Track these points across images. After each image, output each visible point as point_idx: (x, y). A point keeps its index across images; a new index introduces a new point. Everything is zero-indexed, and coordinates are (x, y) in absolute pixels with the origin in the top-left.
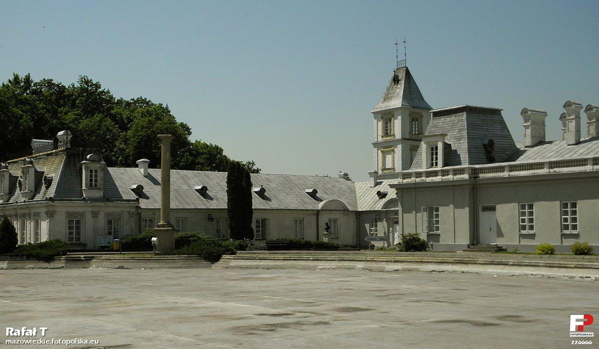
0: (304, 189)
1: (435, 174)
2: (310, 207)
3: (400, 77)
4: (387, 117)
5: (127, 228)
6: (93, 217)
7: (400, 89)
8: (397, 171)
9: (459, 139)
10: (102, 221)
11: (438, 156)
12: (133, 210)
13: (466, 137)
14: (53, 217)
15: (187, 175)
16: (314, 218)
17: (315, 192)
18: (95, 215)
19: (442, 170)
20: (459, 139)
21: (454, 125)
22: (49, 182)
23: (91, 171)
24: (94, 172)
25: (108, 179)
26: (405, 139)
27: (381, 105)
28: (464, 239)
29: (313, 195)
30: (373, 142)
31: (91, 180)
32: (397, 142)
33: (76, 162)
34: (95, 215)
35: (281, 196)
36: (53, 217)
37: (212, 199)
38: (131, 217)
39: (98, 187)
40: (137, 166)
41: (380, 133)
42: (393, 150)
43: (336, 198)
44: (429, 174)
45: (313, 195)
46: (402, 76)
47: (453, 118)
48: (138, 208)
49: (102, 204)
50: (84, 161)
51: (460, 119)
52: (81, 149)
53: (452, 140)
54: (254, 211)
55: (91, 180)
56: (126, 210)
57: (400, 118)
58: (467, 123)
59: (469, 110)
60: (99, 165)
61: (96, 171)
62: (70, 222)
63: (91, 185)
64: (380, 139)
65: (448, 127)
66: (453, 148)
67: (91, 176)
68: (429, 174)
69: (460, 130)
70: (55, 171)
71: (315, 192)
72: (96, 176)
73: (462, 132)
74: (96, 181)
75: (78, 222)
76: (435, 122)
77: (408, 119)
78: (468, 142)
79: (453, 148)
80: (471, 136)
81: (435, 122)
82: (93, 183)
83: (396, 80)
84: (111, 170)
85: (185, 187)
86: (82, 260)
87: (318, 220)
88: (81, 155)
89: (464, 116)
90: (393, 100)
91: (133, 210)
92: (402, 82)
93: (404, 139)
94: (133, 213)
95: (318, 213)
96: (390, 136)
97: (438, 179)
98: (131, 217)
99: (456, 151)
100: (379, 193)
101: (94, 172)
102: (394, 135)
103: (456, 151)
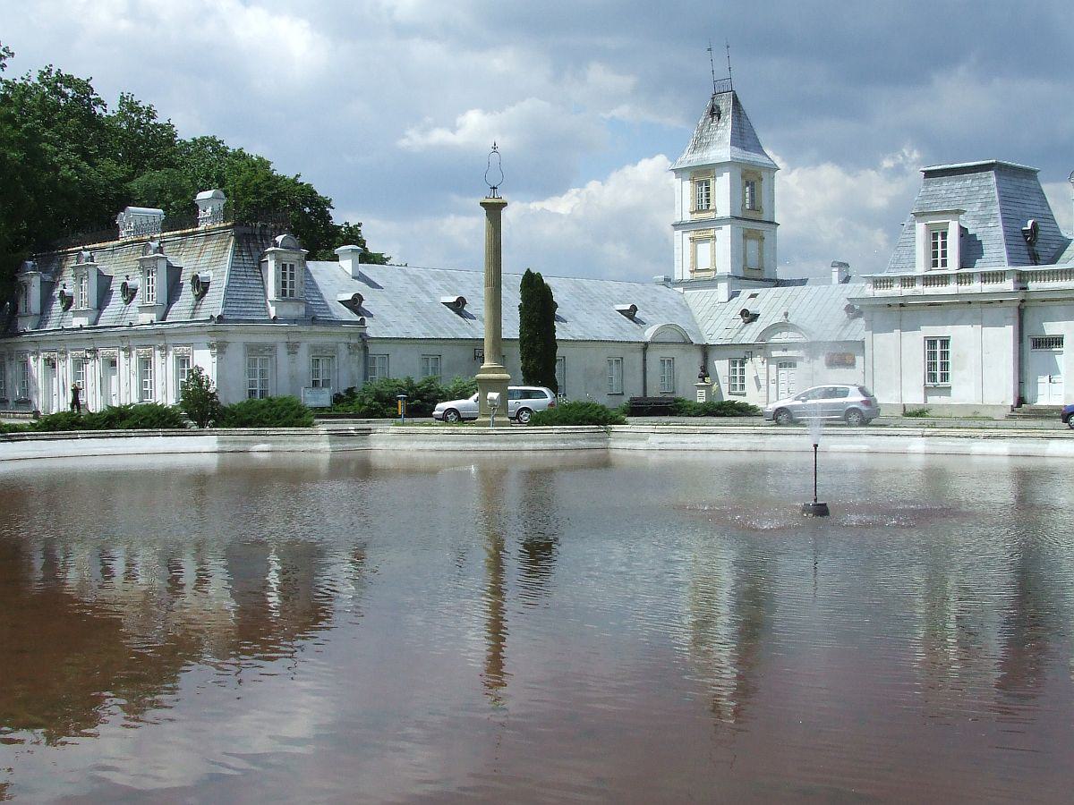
0: (612, 305)
1: (944, 279)
2: (633, 338)
3: (723, 108)
4: (702, 176)
5: (347, 373)
6: (289, 353)
7: (725, 129)
8: (719, 271)
9: (984, 220)
10: (303, 360)
11: (948, 249)
12: (354, 341)
13: (999, 216)
14: (224, 353)
15: (419, 277)
16: (639, 356)
17: (634, 308)
18: (293, 348)
19: (958, 274)
20: (984, 220)
21: (971, 195)
22: (201, 287)
23: (284, 267)
24: (288, 268)
25: (311, 285)
26: (737, 218)
27: (690, 157)
28: (1002, 393)
29: (630, 314)
30: (673, 222)
31: (284, 284)
32: (722, 221)
33: (252, 249)
34: (293, 348)
35: (582, 316)
36: (224, 353)
37: (472, 317)
38: (350, 354)
39: (296, 296)
40: (335, 258)
41: (688, 204)
42: (714, 238)
43: (666, 321)
44: (928, 280)
45: (630, 314)
46: (725, 105)
47: (969, 182)
48: (364, 338)
49: (304, 329)
50: (273, 248)
51: (984, 184)
52: (259, 225)
53: (969, 222)
54: (557, 343)
55: (284, 284)
56: (344, 340)
57: (727, 176)
58: (999, 192)
59: (998, 168)
60: (297, 256)
61: (292, 267)
62: (945, 377)
63: (284, 293)
64: (688, 218)
65: (958, 198)
66: (970, 232)
67: (284, 275)
68: (928, 280)
69: (985, 205)
70: (212, 265)
71: (634, 308)
72: (292, 276)
73: (991, 207)
74: (292, 285)
75: (932, 377)
76: (930, 189)
77: (740, 182)
78: (1004, 227)
79: (970, 232)
80: (1007, 216)
81: (930, 189)
82: (288, 289)
83: (715, 112)
84: (311, 265)
85: (426, 299)
86: (352, 435)
87: (645, 360)
88: (259, 238)
89: (992, 178)
90: (711, 148)
91: (354, 341)
92: (729, 117)
93: (734, 218)
94: (355, 346)
95: (646, 346)
96: (707, 210)
97: (952, 288)
98: (350, 354)
99: (974, 235)
100: (744, 313)
101: (288, 268)
102: (715, 210)
103: (974, 235)
